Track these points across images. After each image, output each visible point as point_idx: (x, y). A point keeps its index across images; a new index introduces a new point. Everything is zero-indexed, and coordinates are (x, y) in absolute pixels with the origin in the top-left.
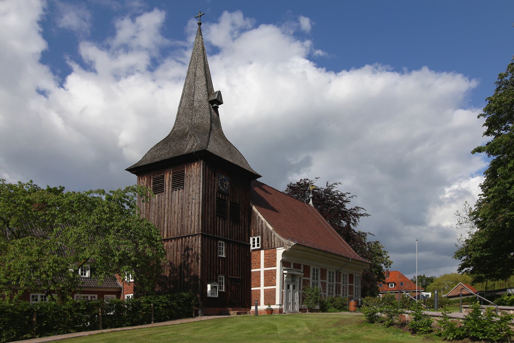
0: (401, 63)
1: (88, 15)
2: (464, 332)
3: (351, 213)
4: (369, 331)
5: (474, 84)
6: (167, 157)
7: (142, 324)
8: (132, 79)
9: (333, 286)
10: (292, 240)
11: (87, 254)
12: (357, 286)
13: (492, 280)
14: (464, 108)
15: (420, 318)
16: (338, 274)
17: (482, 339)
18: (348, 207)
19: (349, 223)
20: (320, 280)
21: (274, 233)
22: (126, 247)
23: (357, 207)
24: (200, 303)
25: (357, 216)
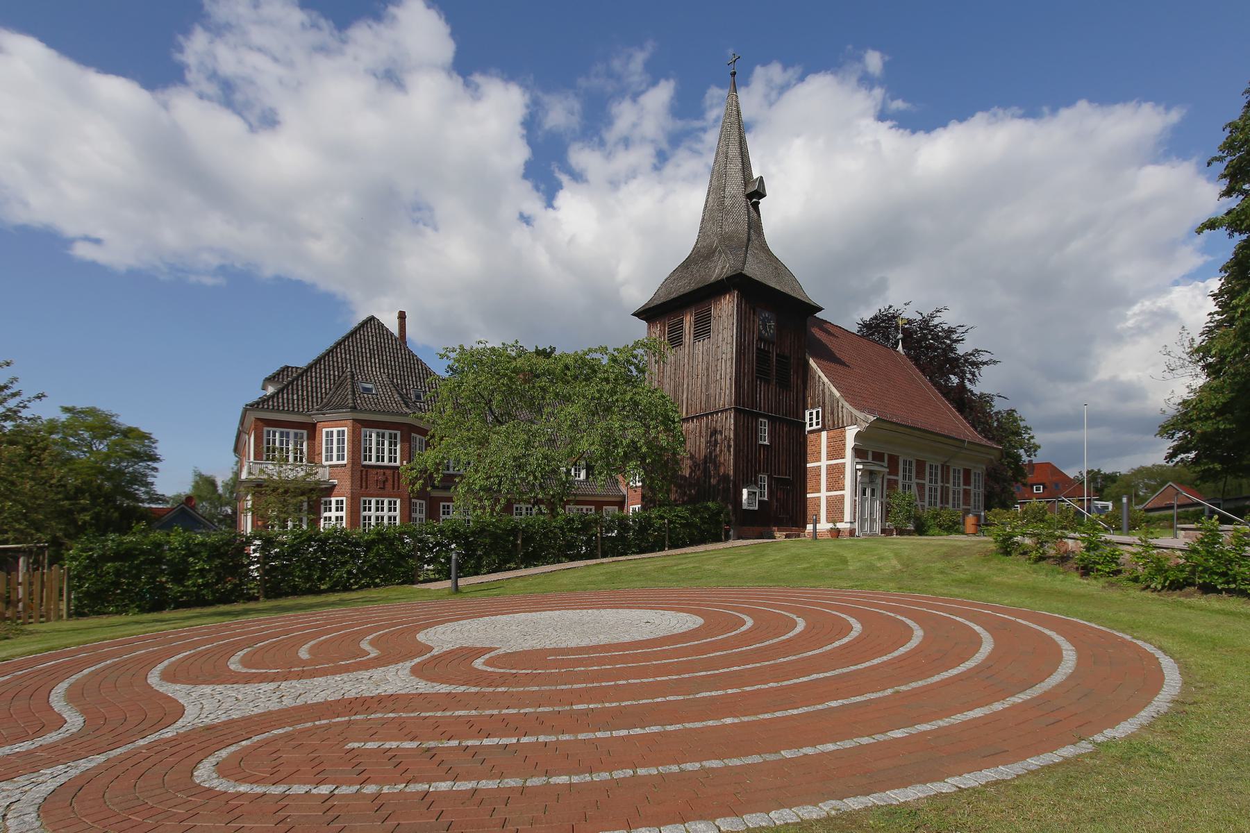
0: (1035, 97)
1: (577, 106)
2: (1184, 575)
3: (966, 361)
4: (1002, 569)
5: (1174, 116)
6: (688, 289)
7: (653, 551)
8: (634, 185)
9: (936, 490)
10: (870, 413)
11: (584, 446)
12: (977, 490)
13: (1237, 477)
14: (1156, 161)
15: (1096, 548)
16: (945, 468)
17: (1223, 589)
18: (961, 349)
19: (962, 378)
20: (914, 480)
21: (842, 402)
22: (634, 432)
23: (977, 351)
24: (733, 518)
25: (974, 364)
